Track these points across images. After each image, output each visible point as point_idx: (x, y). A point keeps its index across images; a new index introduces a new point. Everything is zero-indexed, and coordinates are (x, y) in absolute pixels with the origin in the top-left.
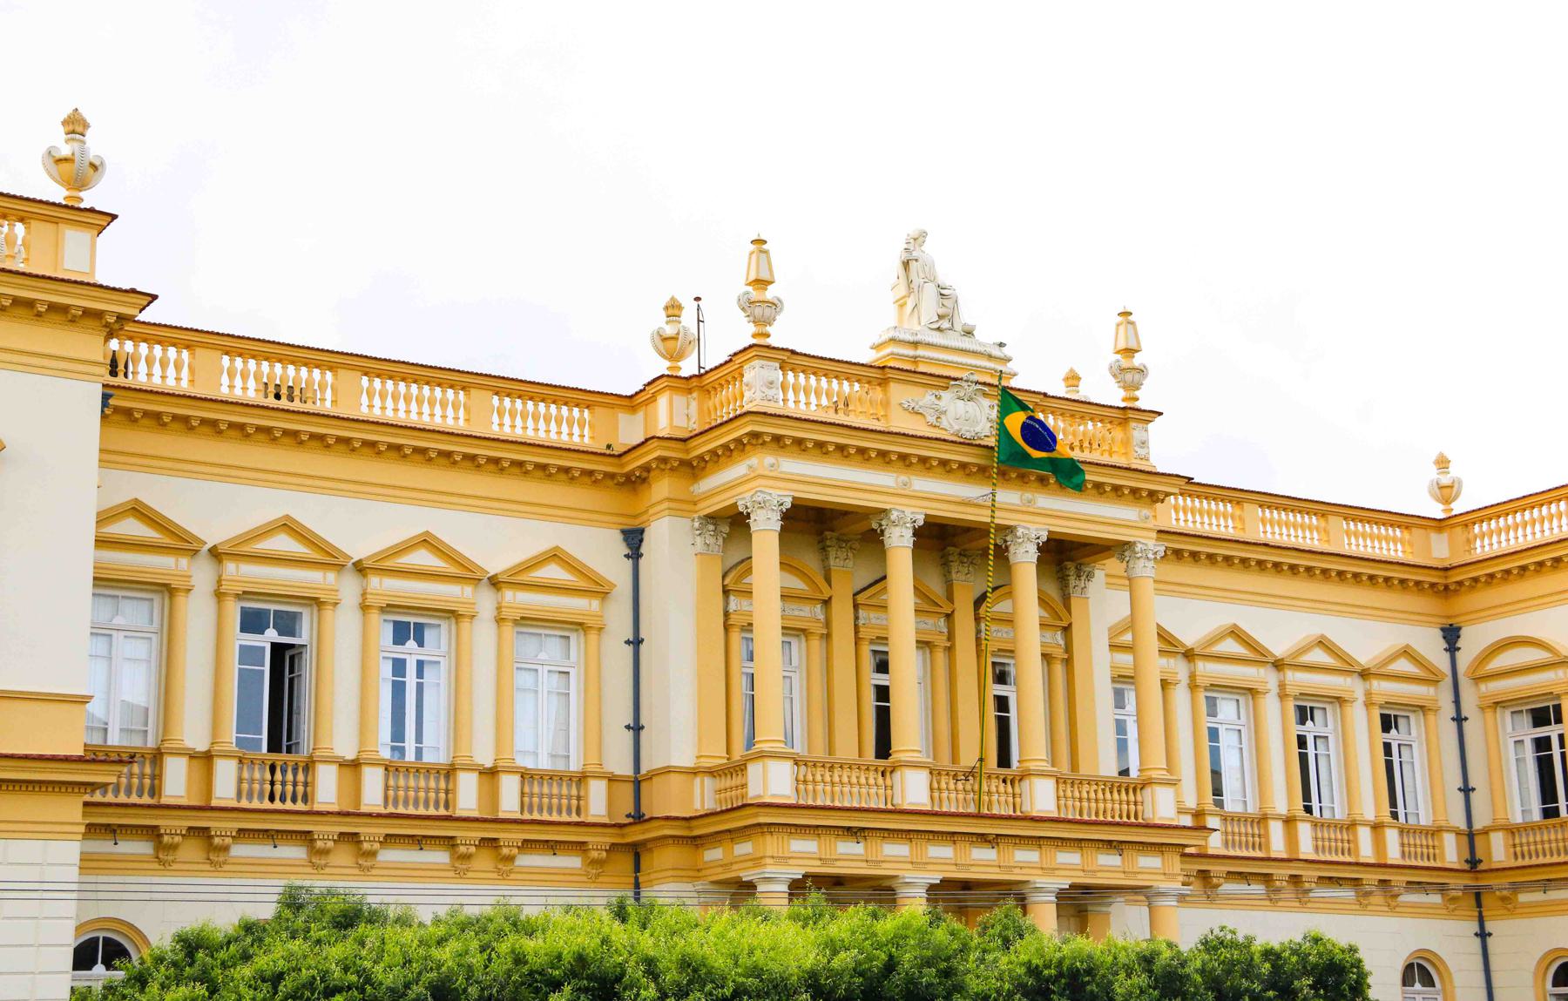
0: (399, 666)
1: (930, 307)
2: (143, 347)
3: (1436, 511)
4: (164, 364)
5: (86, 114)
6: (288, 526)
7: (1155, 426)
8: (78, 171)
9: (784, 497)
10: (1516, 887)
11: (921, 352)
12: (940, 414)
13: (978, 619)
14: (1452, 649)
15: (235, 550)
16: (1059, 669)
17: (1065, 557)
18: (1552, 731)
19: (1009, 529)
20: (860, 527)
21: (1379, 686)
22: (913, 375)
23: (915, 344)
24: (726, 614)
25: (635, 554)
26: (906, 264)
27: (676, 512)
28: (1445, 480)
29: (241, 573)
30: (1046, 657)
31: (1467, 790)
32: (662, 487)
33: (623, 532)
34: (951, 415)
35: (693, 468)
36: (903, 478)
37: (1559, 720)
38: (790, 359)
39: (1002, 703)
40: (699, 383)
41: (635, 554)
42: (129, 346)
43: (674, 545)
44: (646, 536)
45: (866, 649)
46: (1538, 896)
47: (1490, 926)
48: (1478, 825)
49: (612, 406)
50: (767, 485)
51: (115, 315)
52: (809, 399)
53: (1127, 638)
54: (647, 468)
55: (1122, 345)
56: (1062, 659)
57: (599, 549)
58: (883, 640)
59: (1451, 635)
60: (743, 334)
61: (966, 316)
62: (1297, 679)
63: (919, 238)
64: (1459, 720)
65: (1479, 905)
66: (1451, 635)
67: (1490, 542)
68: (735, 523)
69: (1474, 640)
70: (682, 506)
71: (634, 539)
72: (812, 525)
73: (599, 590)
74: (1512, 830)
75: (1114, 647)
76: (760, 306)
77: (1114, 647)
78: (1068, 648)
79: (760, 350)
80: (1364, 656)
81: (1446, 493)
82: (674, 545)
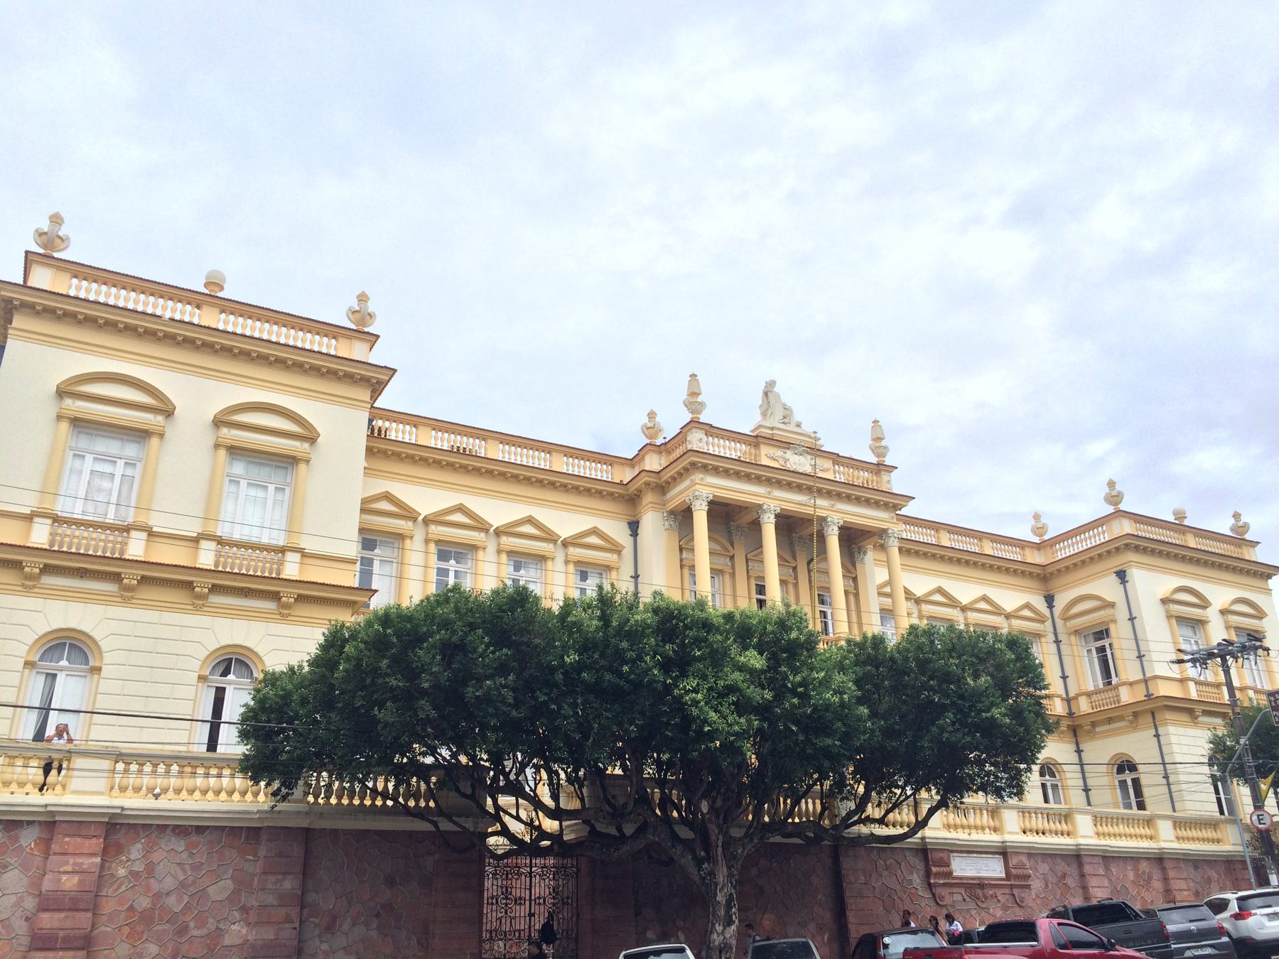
1: (779, 414)
2: (394, 425)
3: (1037, 540)
4: (403, 432)
6: (461, 509)
7: (894, 474)
8: (362, 315)
10: (1094, 724)
12: (787, 460)
13: (809, 571)
14: (1050, 605)
16: (852, 598)
17: (853, 539)
18: (1106, 643)
19: (824, 519)
22: (772, 441)
23: (772, 429)
24: (681, 560)
26: (766, 394)
28: (1039, 525)
29: (437, 531)
30: (846, 593)
31: (1064, 677)
32: (649, 498)
35: (662, 489)
37: (1108, 636)
38: (711, 430)
39: (824, 614)
42: (387, 424)
43: (652, 522)
45: (753, 583)
46: (1106, 727)
47: (1082, 747)
48: (1072, 694)
50: (702, 490)
51: (374, 380)
53: (888, 590)
56: (854, 593)
57: (617, 530)
58: (763, 578)
59: (1050, 600)
60: (687, 417)
61: (797, 416)
63: (771, 384)
64: (1057, 642)
65: (1075, 735)
66: (1050, 600)
67: (1064, 551)
68: (683, 517)
69: (1061, 601)
71: (634, 527)
73: (616, 549)
74: (1089, 695)
75: (880, 594)
76: (693, 400)
77: (880, 594)
78: (856, 588)
79: (694, 424)
80: (1009, 607)
81: (1039, 530)
82: (652, 522)
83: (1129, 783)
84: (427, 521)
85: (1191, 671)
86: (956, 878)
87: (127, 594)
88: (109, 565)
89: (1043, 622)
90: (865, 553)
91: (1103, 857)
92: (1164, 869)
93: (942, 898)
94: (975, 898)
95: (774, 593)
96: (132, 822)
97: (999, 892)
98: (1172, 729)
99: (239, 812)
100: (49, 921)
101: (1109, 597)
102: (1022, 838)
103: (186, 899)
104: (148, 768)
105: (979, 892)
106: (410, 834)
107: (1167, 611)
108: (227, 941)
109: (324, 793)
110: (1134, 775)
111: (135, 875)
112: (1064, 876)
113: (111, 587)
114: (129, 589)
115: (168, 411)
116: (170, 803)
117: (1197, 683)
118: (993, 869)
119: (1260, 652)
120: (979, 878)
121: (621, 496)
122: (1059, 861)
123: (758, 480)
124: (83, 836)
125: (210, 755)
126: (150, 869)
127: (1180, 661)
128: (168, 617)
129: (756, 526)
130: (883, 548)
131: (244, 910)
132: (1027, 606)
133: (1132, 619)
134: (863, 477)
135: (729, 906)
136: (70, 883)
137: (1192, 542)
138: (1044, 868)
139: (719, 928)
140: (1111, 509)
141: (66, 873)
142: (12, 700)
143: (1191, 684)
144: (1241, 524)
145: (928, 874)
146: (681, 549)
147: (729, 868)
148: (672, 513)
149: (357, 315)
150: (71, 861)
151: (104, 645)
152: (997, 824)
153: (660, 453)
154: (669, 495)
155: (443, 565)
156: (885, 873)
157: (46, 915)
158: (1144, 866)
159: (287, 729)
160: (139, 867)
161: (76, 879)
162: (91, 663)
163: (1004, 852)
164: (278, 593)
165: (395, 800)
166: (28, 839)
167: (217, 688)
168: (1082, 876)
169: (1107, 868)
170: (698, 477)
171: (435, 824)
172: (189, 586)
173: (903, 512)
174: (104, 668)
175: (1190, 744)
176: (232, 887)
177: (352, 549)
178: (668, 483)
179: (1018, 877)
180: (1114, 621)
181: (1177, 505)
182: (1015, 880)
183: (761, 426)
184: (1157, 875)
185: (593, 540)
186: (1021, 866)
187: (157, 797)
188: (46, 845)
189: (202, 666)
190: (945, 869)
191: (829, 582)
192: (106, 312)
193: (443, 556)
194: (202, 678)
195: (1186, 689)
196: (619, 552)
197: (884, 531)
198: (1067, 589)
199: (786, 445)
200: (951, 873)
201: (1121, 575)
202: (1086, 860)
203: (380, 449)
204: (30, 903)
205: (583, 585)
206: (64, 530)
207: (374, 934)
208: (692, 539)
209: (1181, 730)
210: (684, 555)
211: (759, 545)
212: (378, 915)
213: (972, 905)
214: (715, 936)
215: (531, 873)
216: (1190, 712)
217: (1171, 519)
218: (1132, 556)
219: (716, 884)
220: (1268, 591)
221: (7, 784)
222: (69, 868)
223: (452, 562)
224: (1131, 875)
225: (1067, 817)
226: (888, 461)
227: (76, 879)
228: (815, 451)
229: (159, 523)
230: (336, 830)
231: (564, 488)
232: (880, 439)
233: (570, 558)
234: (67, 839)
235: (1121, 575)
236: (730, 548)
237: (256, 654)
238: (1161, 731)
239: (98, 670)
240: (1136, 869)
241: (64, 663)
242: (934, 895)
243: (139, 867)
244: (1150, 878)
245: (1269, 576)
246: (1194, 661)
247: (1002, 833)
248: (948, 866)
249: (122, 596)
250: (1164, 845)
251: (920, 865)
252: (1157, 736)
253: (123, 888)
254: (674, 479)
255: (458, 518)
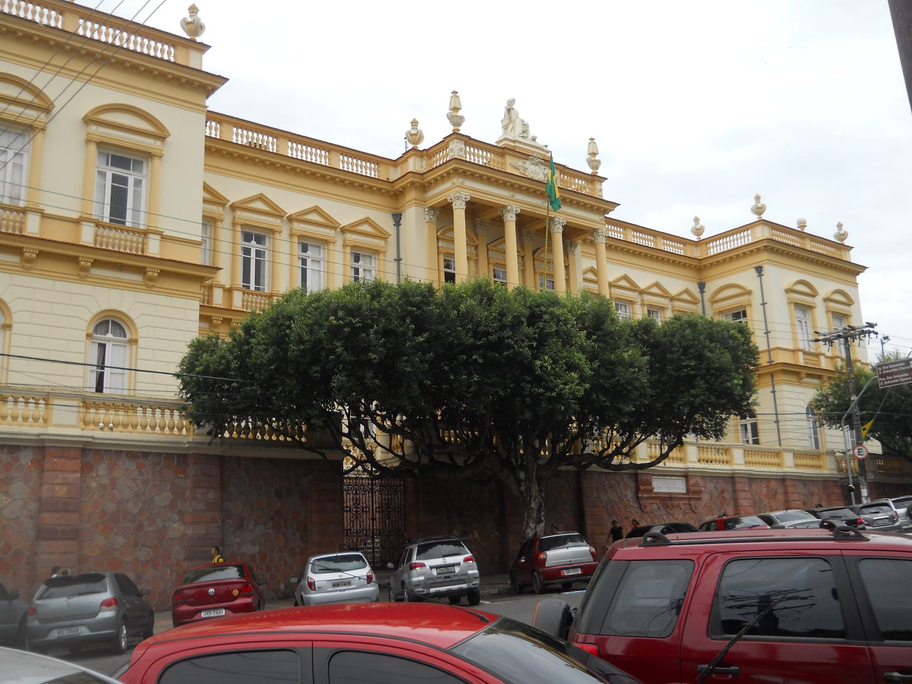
0: (304, 262)
1: (519, 129)
3: (695, 238)
5: (197, 5)
6: (261, 198)
8: (194, 27)
9: (466, 195)
11: (517, 144)
12: (525, 169)
15: (241, 206)
17: (572, 234)
19: (552, 219)
20: (493, 215)
21: (677, 304)
23: (514, 141)
25: (397, 224)
26: (509, 110)
27: (417, 205)
29: (648, 298)
32: (412, 195)
33: (393, 215)
34: (529, 170)
36: (512, 193)
37: (745, 316)
38: (469, 141)
40: (428, 154)
41: (397, 224)
44: (403, 217)
49: (387, 164)
50: (458, 193)
52: (480, 158)
54: (404, 188)
55: (591, 151)
57: (384, 220)
59: (702, 286)
60: (449, 129)
61: (532, 132)
62: (648, 298)
63: (511, 102)
66: (702, 286)
67: (715, 249)
68: (444, 211)
69: (712, 287)
70: (420, 202)
71: (397, 218)
72: (475, 210)
75: (585, 280)
79: (456, 135)
80: (673, 292)
81: (698, 231)
82: (415, 217)
83: (749, 427)
84: (233, 208)
85: (824, 348)
86: (656, 493)
87: (150, 284)
88: (111, 256)
89: (385, 239)
90: (576, 246)
91: (84, 451)
92: (785, 487)
93: (645, 507)
94: (666, 506)
95: (514, 280)
96: (97, 448)
97: (681, 502)
98: (784, 387)
99: (173, 443)
100: (50, 519)
101: (748, 286)
102: (698, 465)
103: (140, 505)
104: (167, 412)
105: (669, 503)
106: (290, 462)
107: (827, 307)
108: (171, 535)
109: (241, 428)
110: (753, 420)
111: (103, 487)
112: (723, 492)
113: (138, 278)
114: (151, 279)
115: (47, 109)
116: (118, 434)
117: (805, 353)
118: (678, 487)
119: (872, 334)
120: (669, 493)
121: (388, 192)
122: (721, 481)
123: (504, 185)
124: (66, 458)
125: (98, 395)
126: (113, 483)
127: (817, 340)
128: (61, 285)
129: (499, 222)
130: (592, 243)
131: (181, 513)
132: (686, 291)
133: (763, 304)
134: (165, 52)
135: (539, 511)
136: (62, 492)
137: (809, 245)
138: (711, 486)
139: (532, 525)
140: (755, 218)
141: (58, 484)
142: (12, 360)
143: (801, 354)
144: (842, 232)
145: (637, 490)
146: (438, 239)
147: (539, 485)
148: (432, 208)
149: (190, 26)
150: (60, 476)
151: (138, 322)
152: (683, 456)
153: (422, 157)
154: (431, 193)
155: (247, 245)
156: (610, 490)
157: (46, 515)
158: (773, 484)
159: (216, 383)
160: (106, 481)
161: (65, 489)
162: (128, 337)
163: (686, 475)
164: (145, 268)
165: (293, 437)
166: (26, 458)
167: (100, 344)
168: (735, 491)
169: (750, 486)
170: (457, 180)
171: (323, 455)
172: (74, 260)
173: (611, 215)
174: (140, 341)
175: (796, 398)
176: (171, 497)
177: (195, 232)
178: (430, 183)
179: (695, 492)
180: (750, 305)
181: (801, 216)
182: (693, 494)
183: (506, 139)
184: (781, 490)
185: (366, 228)
186: (697, 485)
187: (111, 429)
188: (39, 464)
189: (88, 328)
190: (649, 487)
191: (453, 249)
192: (58, 36)
193: (247, 237)
194: (89, 336)
195: (797, 358)
196: (385, 239)
197: (595, 230)
198: (719, 278)
199: (525, 156)
200: (652, 490)
201: (759, 270)
202: (738, 480)
203: (216, 150)
204: (33, 506)
205: (356, 265)
206: (169, 245)
207: (270, 531)
208: (452, 229)
209: (791, 388)
210: (440, 244)
211: (501, 237)
212: (272, 519)
213: (664, 512)
214: (529, 530)
215: (372, 489)
216: (797, 374)
217: (795, 226)
218: (764, 256)
219: (531, 497)
220: (856, 285)
221: (4, 418)
222: (59, 481)
223: (253, 242)
224: (765, 491)
225: (727, 450)
226: (600, 173)
227: (65, 489)
228: (548, 162)
229: (169, 227)
230: (291, 460)
231: (343, 183)
232: (594, 154)
233: (347, 243)
234: (55, 460)
235: (759, 270)
236: (475, 239)
237: (125, 314)
238: (777, 388)
239: (134, 342)
240: (768, 486)
241: (109, 335)
242: (640, 505)
243: (106, 481)
244: (776, 492)
245: (858, 274)
246: (825, 340)
247: (686, 463)
248: (650, 484)
249: (23, 267)
250: (786, 470)
251: (632, 484)
252: (774, 392)
253: (96, 496)
254: (436, 180)
255: (314, 217)
